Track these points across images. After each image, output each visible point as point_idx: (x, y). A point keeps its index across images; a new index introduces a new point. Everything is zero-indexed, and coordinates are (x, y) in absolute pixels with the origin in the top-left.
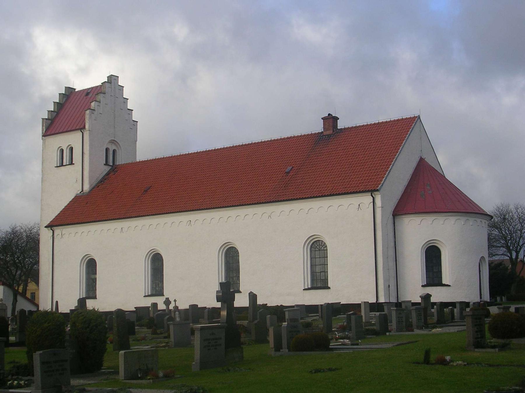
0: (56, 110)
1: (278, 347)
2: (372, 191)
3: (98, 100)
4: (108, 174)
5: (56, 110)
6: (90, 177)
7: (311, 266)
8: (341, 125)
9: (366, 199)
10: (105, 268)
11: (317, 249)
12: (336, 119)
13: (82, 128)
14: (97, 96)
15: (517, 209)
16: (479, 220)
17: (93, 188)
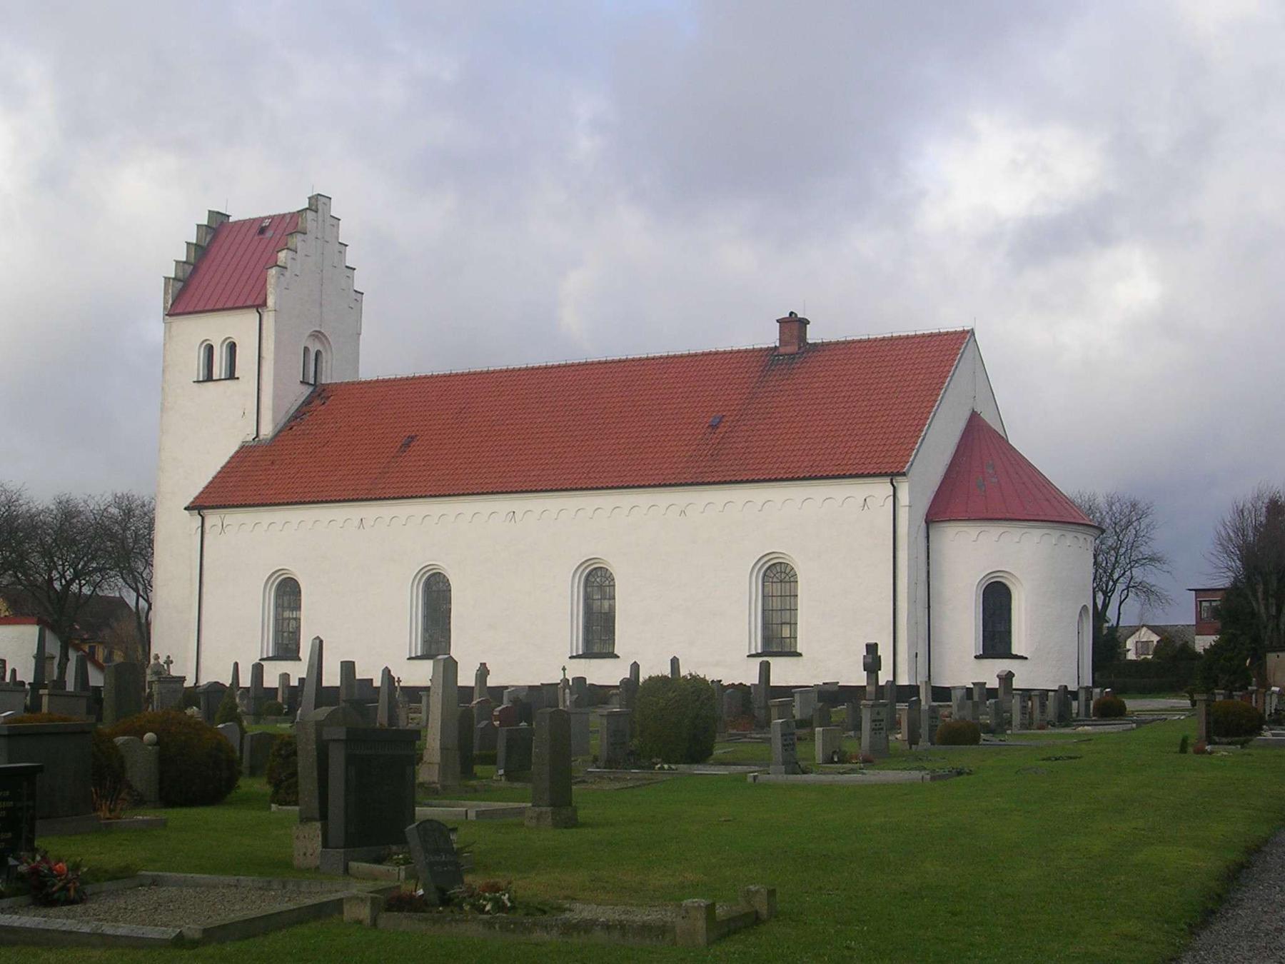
0: (192, 260)
1: (913, 739)
2: (894, 475)
3: (293, 247)
4: (308, 402)
5: (192, 260)
6: (276, 410)
7: (764, 611)
8: (813, 335)
9: (881, 489)
10: (264, 598)
11: (777, 579)
12: (804, 323)
13: (260, 306)
14: (290, 238)
15: (1111, 505)
16: (1081, 537)
17: (280, 431)
